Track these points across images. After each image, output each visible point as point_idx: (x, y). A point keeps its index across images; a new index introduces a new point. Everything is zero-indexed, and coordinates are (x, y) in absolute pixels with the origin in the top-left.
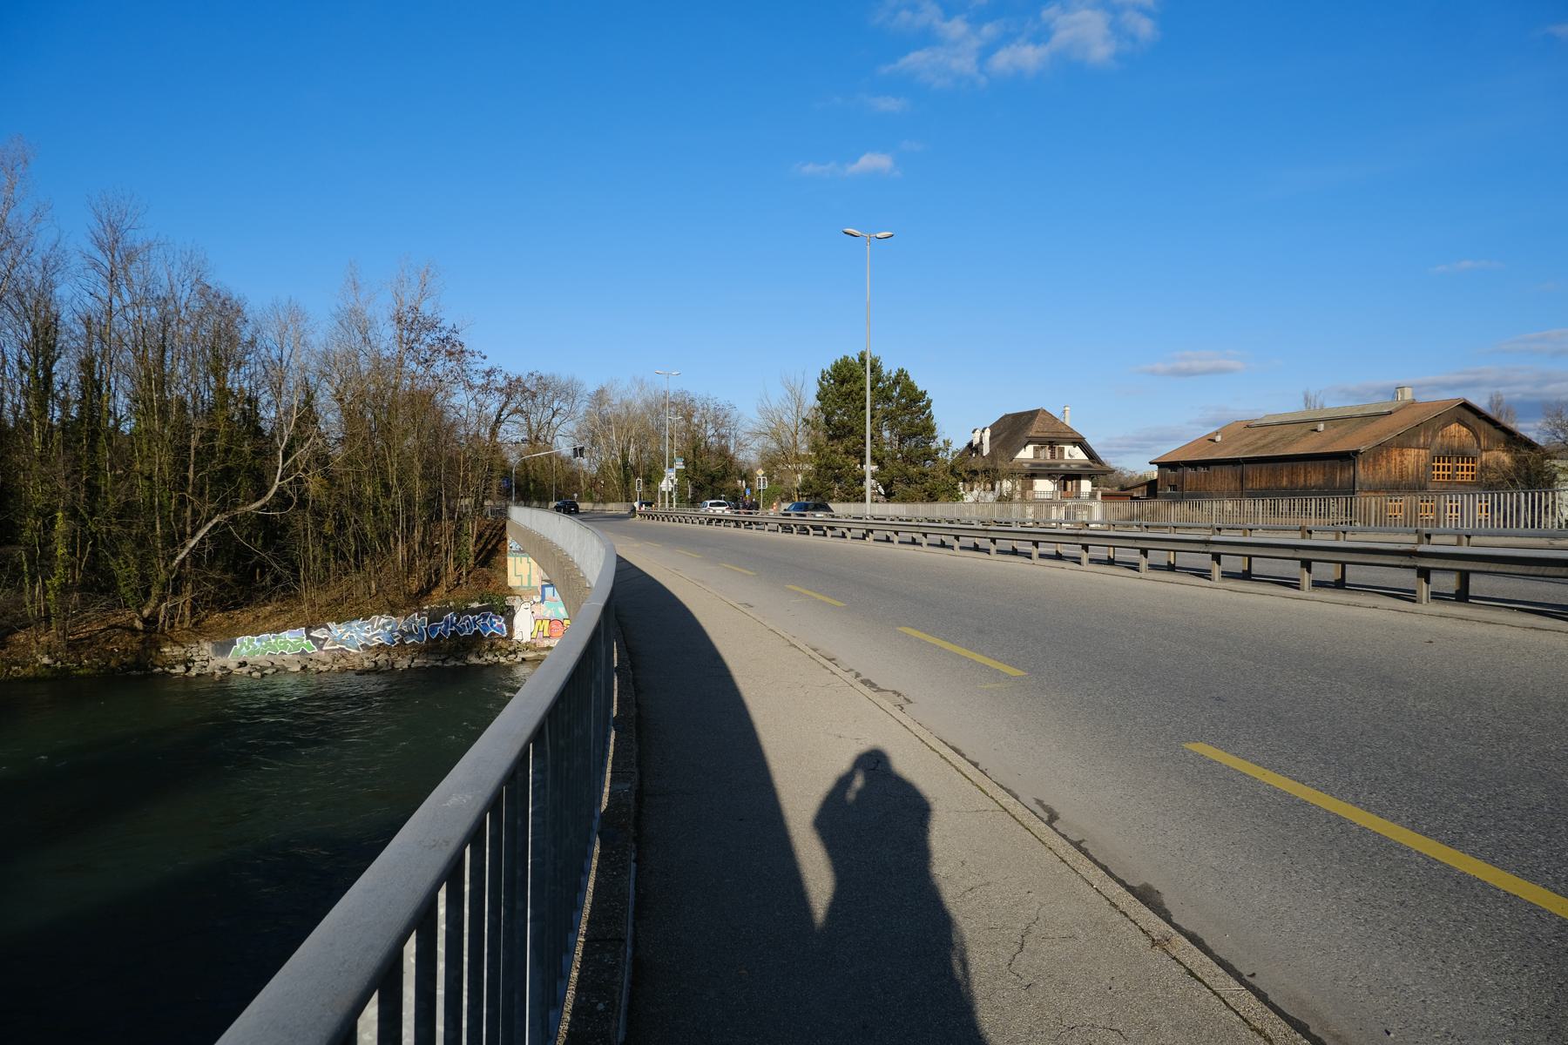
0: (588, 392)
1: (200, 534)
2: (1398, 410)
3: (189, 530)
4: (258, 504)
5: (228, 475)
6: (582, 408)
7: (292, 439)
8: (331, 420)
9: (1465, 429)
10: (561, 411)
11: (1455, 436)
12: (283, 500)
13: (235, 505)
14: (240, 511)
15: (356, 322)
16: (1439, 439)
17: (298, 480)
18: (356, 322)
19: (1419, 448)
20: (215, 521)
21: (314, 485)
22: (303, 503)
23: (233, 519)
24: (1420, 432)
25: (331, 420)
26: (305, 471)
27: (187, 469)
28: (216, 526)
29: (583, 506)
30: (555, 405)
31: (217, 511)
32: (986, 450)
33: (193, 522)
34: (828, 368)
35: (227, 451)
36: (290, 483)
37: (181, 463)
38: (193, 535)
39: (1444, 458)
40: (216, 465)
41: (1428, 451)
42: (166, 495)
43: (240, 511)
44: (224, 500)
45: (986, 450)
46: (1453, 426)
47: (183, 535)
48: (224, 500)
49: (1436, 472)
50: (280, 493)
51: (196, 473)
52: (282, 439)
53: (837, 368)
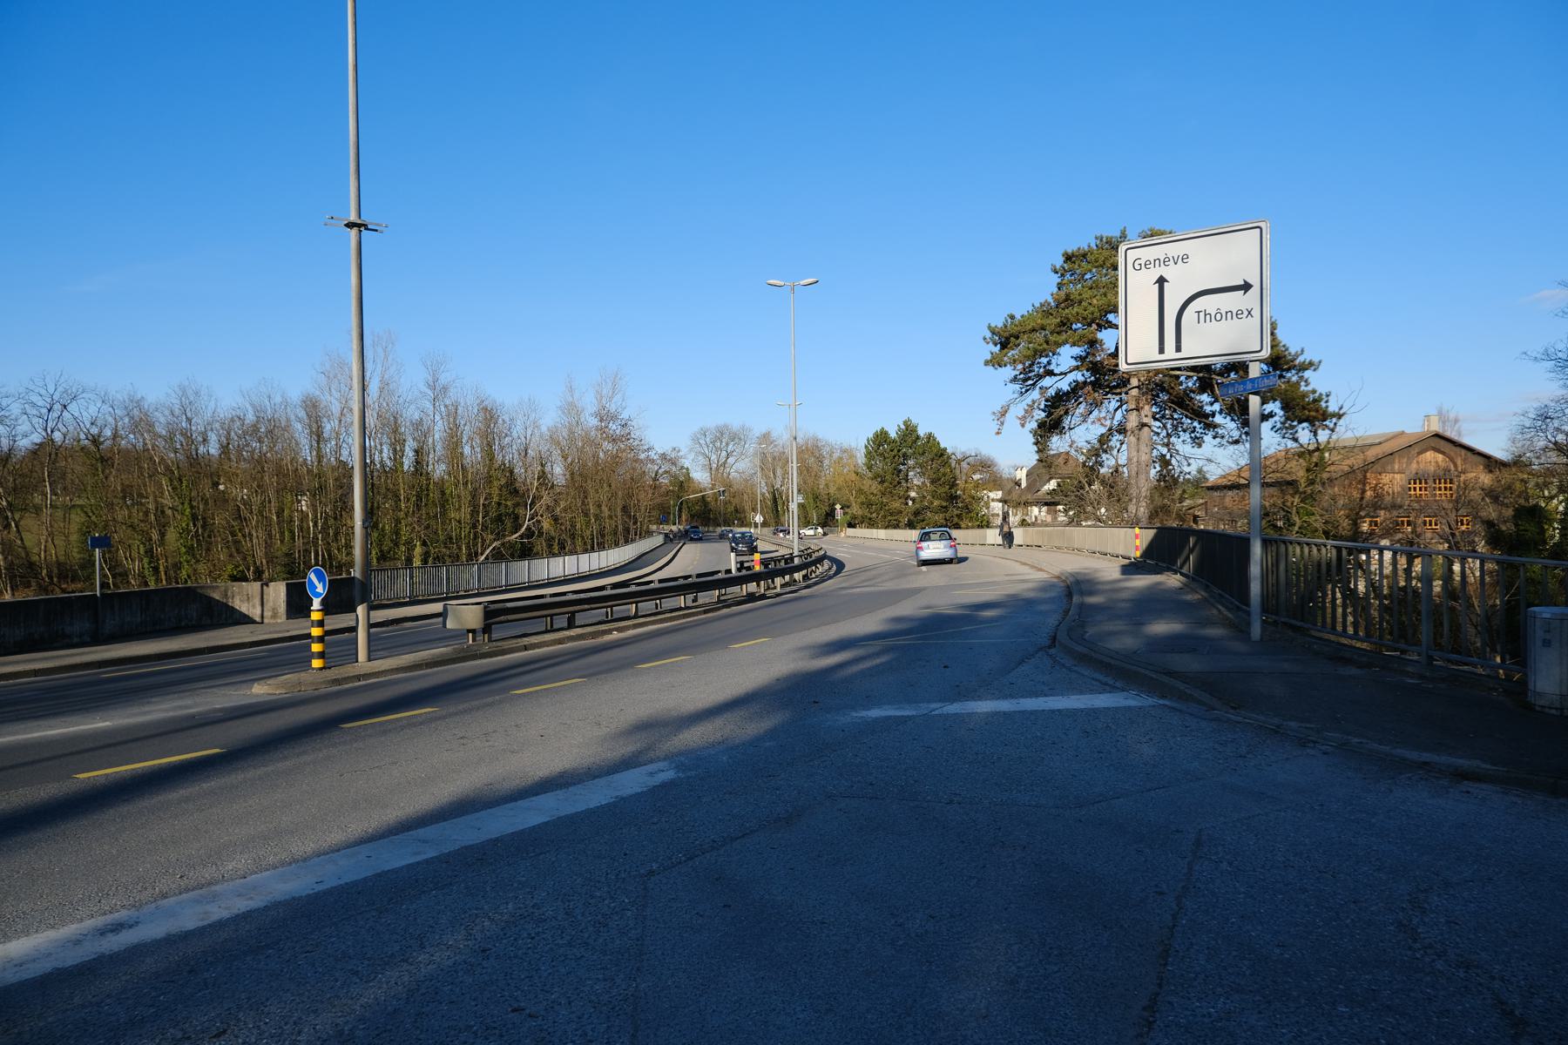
0: (757, 435)
1: (488, 552)
2: (1385, 441)
3: (480, 551)
4: (516, 535)
5: (499, 519)
6: (751, 447)
7: (534, 497)
8: (558, 471)
9: (1440, 455)
10: (735, 453)
11: (1430, 462)
12: (529, 533)
13: (504, 536)
14: (508, 539)
15: (571, 409)
16: (1414, 466)
17: (539, 521)
18: (571, 409)
19: (1394, 473)
20: (494, 545)
21: (546, 525)
22: (541, 534)
23: (503, 544)
24: (1394, 460)
25: (558, 471)
26: (542, 516)
27: (478, 515)
28: (494, 549)
29: (1084, 524)
30: (730, 448)
31: (495, 540)
32: (1024, 485)
33: (482, 546)
34: (871, 436)
35: (499, 504)
36: (533, 523)
37: (474, 512)
38: (482, 554)
39: (1415, 481)
40: (493, 514)
41: (1403, 475)
42: (467, 530)
43: (508, 539)
44: (498, 534)
45: (1024, 485)
46: (1428, 453)
47: (476, 554)
48: (499, 533)
49: (1438, 492)
50: (528, 529)
51: (483, 518)
52: (529, 497)
53: (876, 436)
